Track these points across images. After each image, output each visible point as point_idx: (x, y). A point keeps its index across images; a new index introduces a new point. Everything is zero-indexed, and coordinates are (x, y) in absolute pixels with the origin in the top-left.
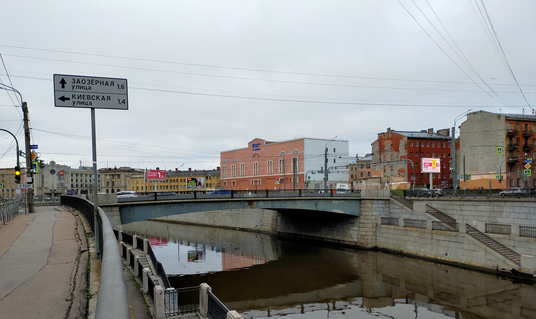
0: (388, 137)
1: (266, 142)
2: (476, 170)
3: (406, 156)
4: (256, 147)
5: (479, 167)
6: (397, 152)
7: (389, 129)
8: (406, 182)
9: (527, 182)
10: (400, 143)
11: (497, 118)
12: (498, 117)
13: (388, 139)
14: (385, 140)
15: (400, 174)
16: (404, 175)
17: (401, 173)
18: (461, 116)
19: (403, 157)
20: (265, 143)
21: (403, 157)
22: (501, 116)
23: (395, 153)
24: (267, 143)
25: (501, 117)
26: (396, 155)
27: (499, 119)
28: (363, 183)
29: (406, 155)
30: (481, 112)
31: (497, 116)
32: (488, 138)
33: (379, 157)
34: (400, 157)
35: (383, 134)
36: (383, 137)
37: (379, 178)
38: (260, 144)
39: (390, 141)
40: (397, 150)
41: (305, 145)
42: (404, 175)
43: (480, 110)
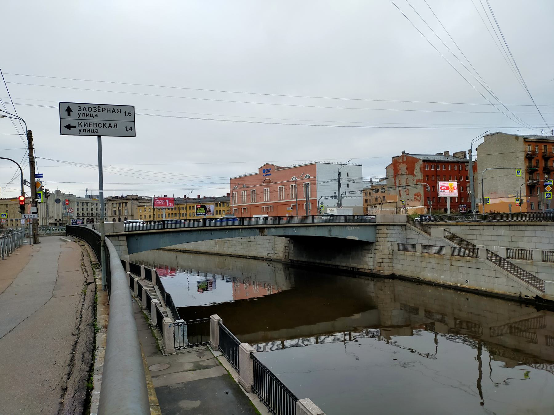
0: (403, 160)
1: (277, 167)
2: (495, 193)
3: (422, 180)
4: (267, 172)
5: (498, 190)
6: (412, 176)
7: (403, 152)
8: (422, 207)
9: (548, 205)
10: (415, 166)
11: (515, 140)
12: (516, 139)
13: (403, 162)
14: (400, 163)
15: (416, 199)
16: (421, 199)
17: (418, 197)
18: (478, 138)
19: (419, 181)
20: (276, 168)
21: (419, 181)
22: (519, 137)
23: (410, 177)
24: (278, 168)
25: (519, 138)
26: (411, 179)
27: (517, 140)
28: (377, 208)
29: (422, 178)
30: (498, 133)
31: (515, 138)
32: (506, 160)
33: (394, 181)
34: (415, 180)
35: (397, 158)
36: (398, 161)
37: (395, 202)
38: (270, 169)
39: (405, 164)
40: (413, 174)
41: (318, 169)
42: (421, 199)
43: (497, 132)
